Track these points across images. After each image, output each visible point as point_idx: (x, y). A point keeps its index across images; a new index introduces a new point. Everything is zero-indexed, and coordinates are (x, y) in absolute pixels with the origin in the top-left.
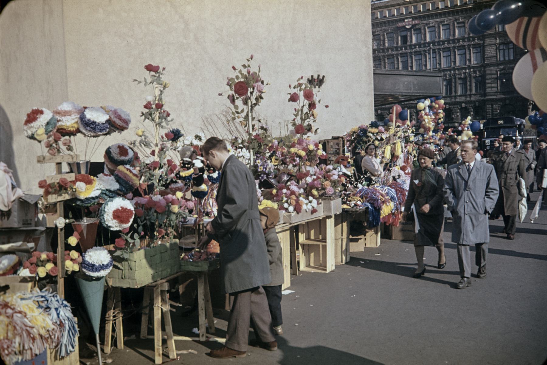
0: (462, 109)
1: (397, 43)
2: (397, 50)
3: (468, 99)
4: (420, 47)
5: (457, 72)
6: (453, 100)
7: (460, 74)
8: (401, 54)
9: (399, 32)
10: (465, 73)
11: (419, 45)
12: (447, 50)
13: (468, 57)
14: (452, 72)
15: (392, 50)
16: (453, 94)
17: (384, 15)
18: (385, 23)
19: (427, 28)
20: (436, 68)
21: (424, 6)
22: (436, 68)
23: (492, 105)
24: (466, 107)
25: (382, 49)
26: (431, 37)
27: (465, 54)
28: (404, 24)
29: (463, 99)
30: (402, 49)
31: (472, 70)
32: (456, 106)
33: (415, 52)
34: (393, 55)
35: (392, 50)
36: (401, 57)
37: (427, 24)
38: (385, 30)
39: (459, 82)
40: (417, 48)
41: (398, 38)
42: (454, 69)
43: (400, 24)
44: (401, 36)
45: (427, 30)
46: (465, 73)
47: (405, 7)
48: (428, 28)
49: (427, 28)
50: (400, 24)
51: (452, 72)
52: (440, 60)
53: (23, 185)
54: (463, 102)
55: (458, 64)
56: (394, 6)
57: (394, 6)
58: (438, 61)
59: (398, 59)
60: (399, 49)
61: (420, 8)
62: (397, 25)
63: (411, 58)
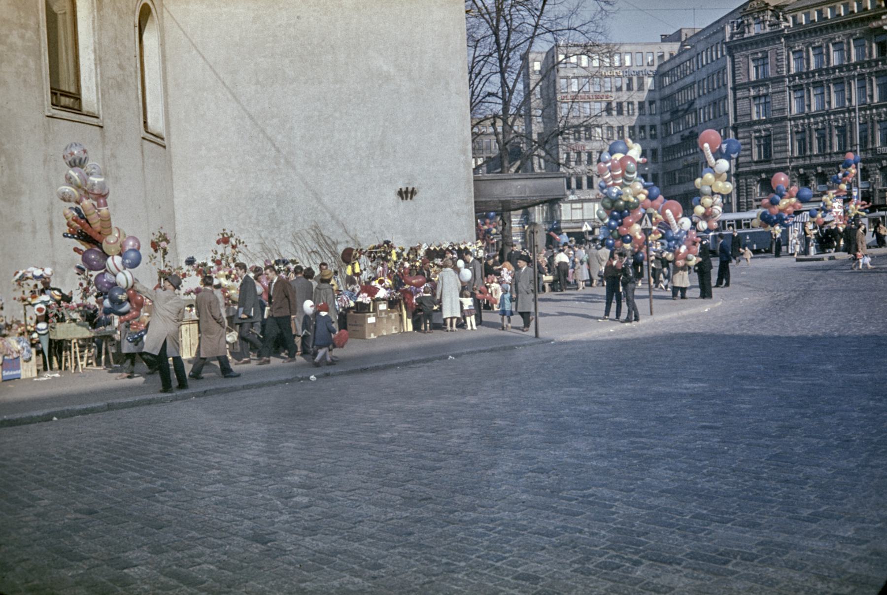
0: (818, 175)
1: (871, 54)
2: (870, 66)
3: (808, 162)
4: (862, 67)
5: (874, 111)
6: (828, 160)
7: (879, 115)
8: (876, 72)
9: (873, 37)
10: (803, 125)
11: (840, 68)
12: (818, 85)
13: (826, 99)
14: (847, 115)
15: (841, 71)
16: (808, 153)
17: (850, 10)
18: (826, 28)
19: (811, 49)
20: (803, 113)
21: (833, 9)
22: (803, 113)
23: (746, 180)
24: (805, 174)
25: (847, 66)
26: (857, 55)
27: (823, 93)
28: (880, 23)
29: (821, 160)
30: (877, 65)
31: (812, 120)
32: (874, 164)
33: (814, 83)
34: (822, 81)
35: (862, 67)
36: (876, 77)
37: (831, 39)
38: (851, 35)
39: (878, 126)
40: (797, 81)
41: (871, 47)
42: (808, 116)
43: (875, 24)
44: (876, 43)
45: (811, 53)
46: (803, 125)
47: (805, 14)
48: (833, 44)
49: (811, 49)
50: (875, 24)
51: (847, 115)
52: (810, 100)
53: (395, 245)
54: (819, 165)
55: (813, 108)
56: (813, 6)
57: (813, 6)
58: (806, 102)
59: (871, 81)
60: (873, 64)
61: (853, 7)
62: (870, 26)
63: (809, 91)
